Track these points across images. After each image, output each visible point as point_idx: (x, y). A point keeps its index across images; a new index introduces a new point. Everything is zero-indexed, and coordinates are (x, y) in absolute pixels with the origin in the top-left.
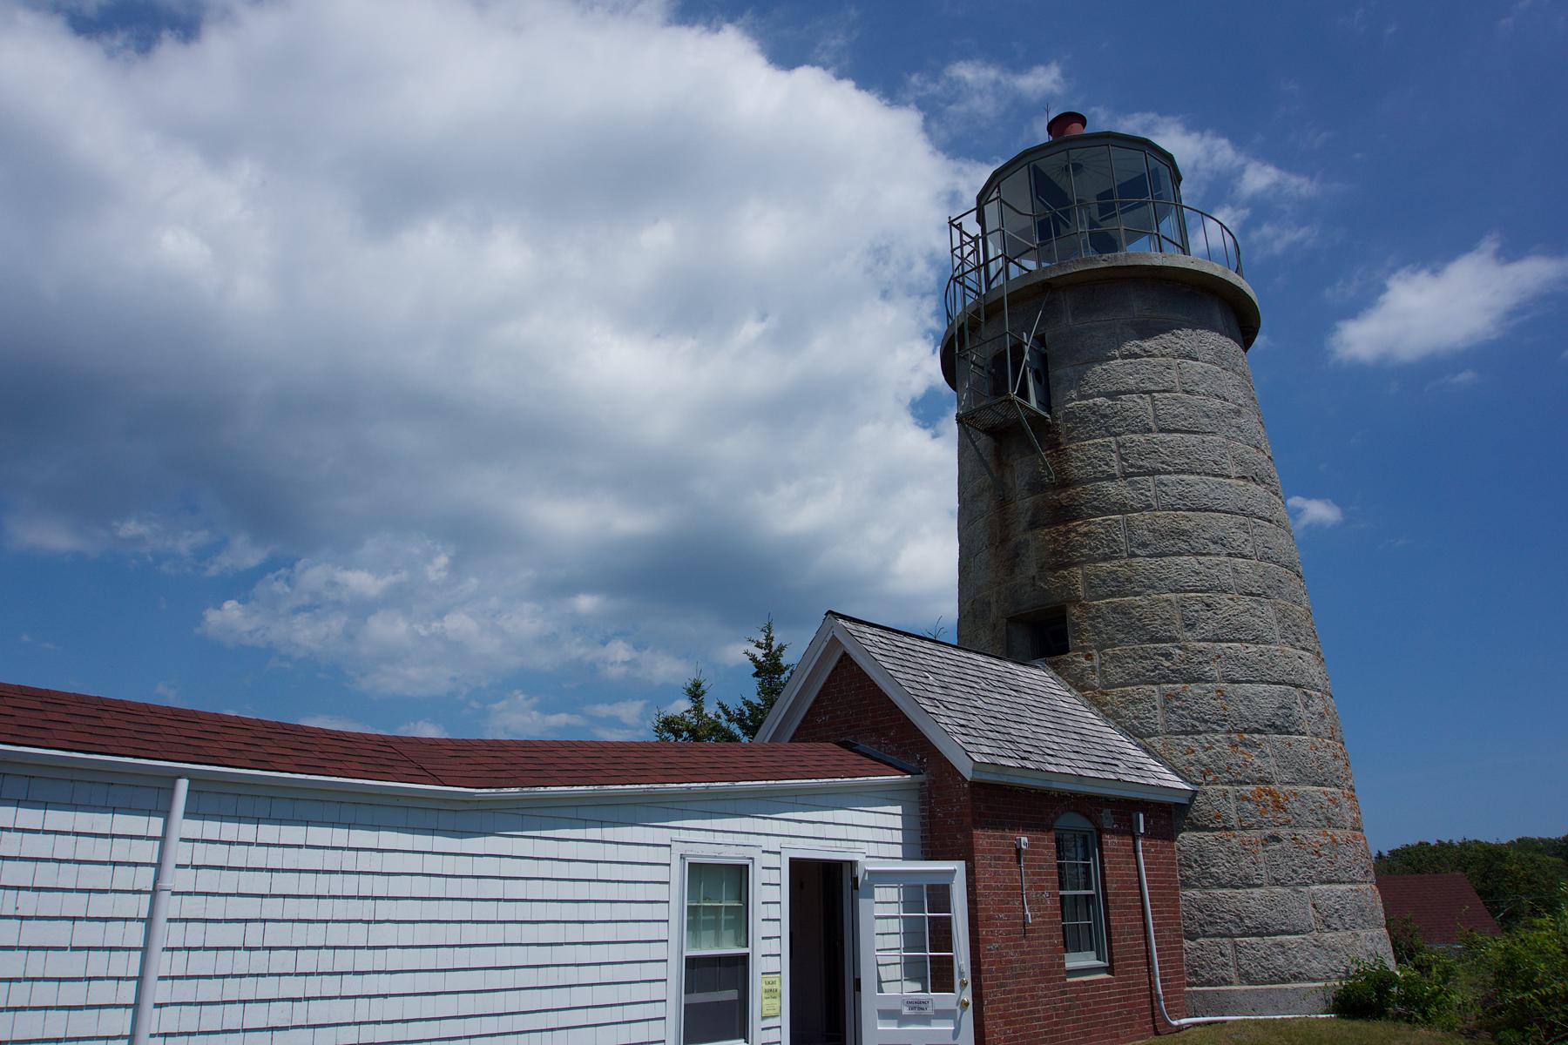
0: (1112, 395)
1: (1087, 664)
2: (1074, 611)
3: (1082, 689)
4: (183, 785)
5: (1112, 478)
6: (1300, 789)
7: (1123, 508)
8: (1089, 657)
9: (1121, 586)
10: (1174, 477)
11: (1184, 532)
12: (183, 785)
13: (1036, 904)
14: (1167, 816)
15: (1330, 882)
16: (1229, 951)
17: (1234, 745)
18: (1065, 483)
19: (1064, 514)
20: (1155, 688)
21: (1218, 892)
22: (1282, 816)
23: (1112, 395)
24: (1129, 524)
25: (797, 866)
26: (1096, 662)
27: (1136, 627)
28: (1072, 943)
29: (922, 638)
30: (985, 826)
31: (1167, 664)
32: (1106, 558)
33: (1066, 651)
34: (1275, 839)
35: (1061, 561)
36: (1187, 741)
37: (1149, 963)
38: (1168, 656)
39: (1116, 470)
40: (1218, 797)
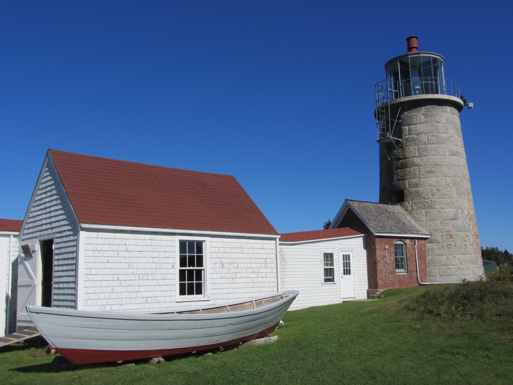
2: (406, 191)
3: (407, 210)
5: (416, 157)
6: (458, 233)
9: (416, 185)
13: (390, 259)
15: (463, 254)
16: (437, 269)
18: (405, 158)
21: (436, 257)
22: (452, 240)
24: (419, 169)
25: (324, 254)
26: (410, 204)
28: (397, 267)
29: (367, 202)
33: (403, 201)
34: (450, 245)
36: (431, 223)
37: (417, 272)
38: (427, 202)
39: (417, 155)
40: (438, 236)
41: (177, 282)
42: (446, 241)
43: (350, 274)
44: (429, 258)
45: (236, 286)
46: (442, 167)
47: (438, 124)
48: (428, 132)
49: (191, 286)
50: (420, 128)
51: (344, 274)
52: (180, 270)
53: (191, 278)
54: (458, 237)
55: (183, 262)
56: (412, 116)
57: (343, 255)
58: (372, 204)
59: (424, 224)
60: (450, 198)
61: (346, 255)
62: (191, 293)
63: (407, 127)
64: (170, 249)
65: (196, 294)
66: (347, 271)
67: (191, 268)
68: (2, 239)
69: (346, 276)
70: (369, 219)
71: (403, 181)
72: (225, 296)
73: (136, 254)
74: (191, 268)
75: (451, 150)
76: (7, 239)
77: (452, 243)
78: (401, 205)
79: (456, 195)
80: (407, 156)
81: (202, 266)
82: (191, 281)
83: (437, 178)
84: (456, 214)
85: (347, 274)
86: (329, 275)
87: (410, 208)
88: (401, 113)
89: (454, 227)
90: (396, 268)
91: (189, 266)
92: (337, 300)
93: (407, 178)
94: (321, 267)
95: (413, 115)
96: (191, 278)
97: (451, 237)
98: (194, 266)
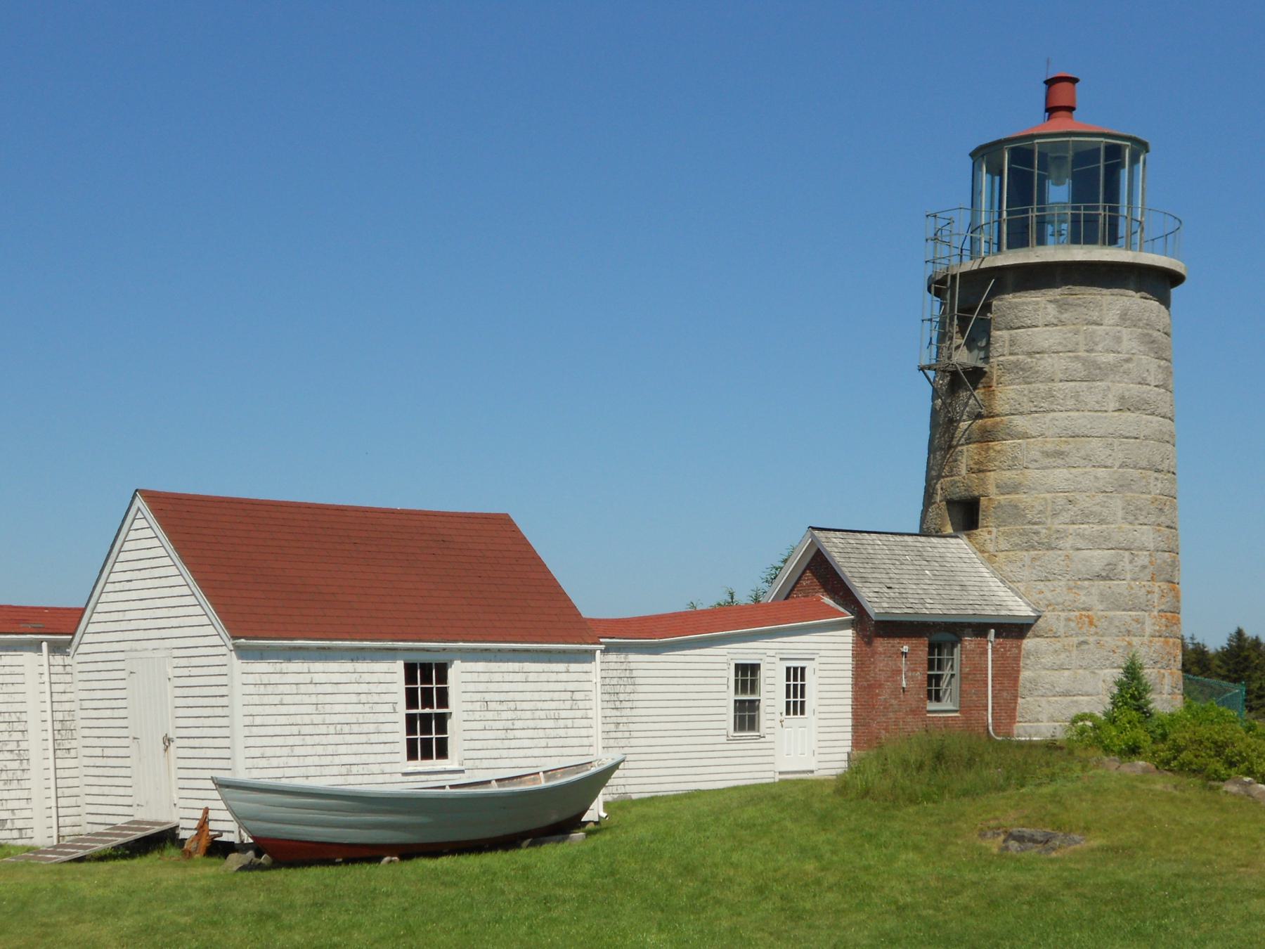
0: (1030, 354)
1: (988, 537)
2: (983, 501)
4: (44, 645)
7: (1025, 436)
8: (990, 532)
9: (1015, 488)
10: (1064, 414)
11: (1062, 453)
12: (44, 645)
14: (1015, 630)
17: (1070, 589)
19: (986, 437)
20: (1025, 553)
21: (1044, 672)
22: (1093, 629)
23: (1030, 354)
25: (737, 666)
26: (994, 535)
27: (1016, 513)
30: (868, 616)
31: (1036, 538)
32: (1010, 468)
35: (979, 469)
36: (1041, 585)
41: (402, 737)
42: (1077, 635)
43: (802, 713)
44: (1025, 675)
45: (513, 744)
46: (1089, 442)
47: (1095, 327)
48: (1060, 348)
49: (427, 744)
50: (1043, 337)
51: (788, 713)
52: (408, 715)
53: (426, 729)
54: (1111, 623)
55: (411, 701)
56: (1023, 303)
57: (788, 669)
58: (883, 537)
59: (1022, 589)
60: (1101, 522)
61: (795, 669)
62: (427, 755)
63: (1005, 334)
64: (388, 678)
65: (438, 757)
66: (795, 705)
67: (427, 710)
68: (9, 658)
69: (794, 720)
70: (864, 580)
71: (981, 475)
72: (492, 763)
73: (329, 688)
74: (427, 710)
75: (1123, 398)
76: (27, 657)
77: (1091, 639)
78: (969, 536)
79: (1120, 514)
80: (998, 409)
81: (446, 706)
82: (427, 734)
83: (1073, 470)
84: (1111, 566)
85: (795, 713)
86: (746, 716)
87: (991, 547)
88: (993, 294)
89: (1103, 597)
90: (930, 698)
91: (423, 707)
92: (767, 775)
93: (991, 466)
94: (730, 696)
95: (1027, 304)
96: (426, 729)
97: (1091, 623)
98: (432, 707)
